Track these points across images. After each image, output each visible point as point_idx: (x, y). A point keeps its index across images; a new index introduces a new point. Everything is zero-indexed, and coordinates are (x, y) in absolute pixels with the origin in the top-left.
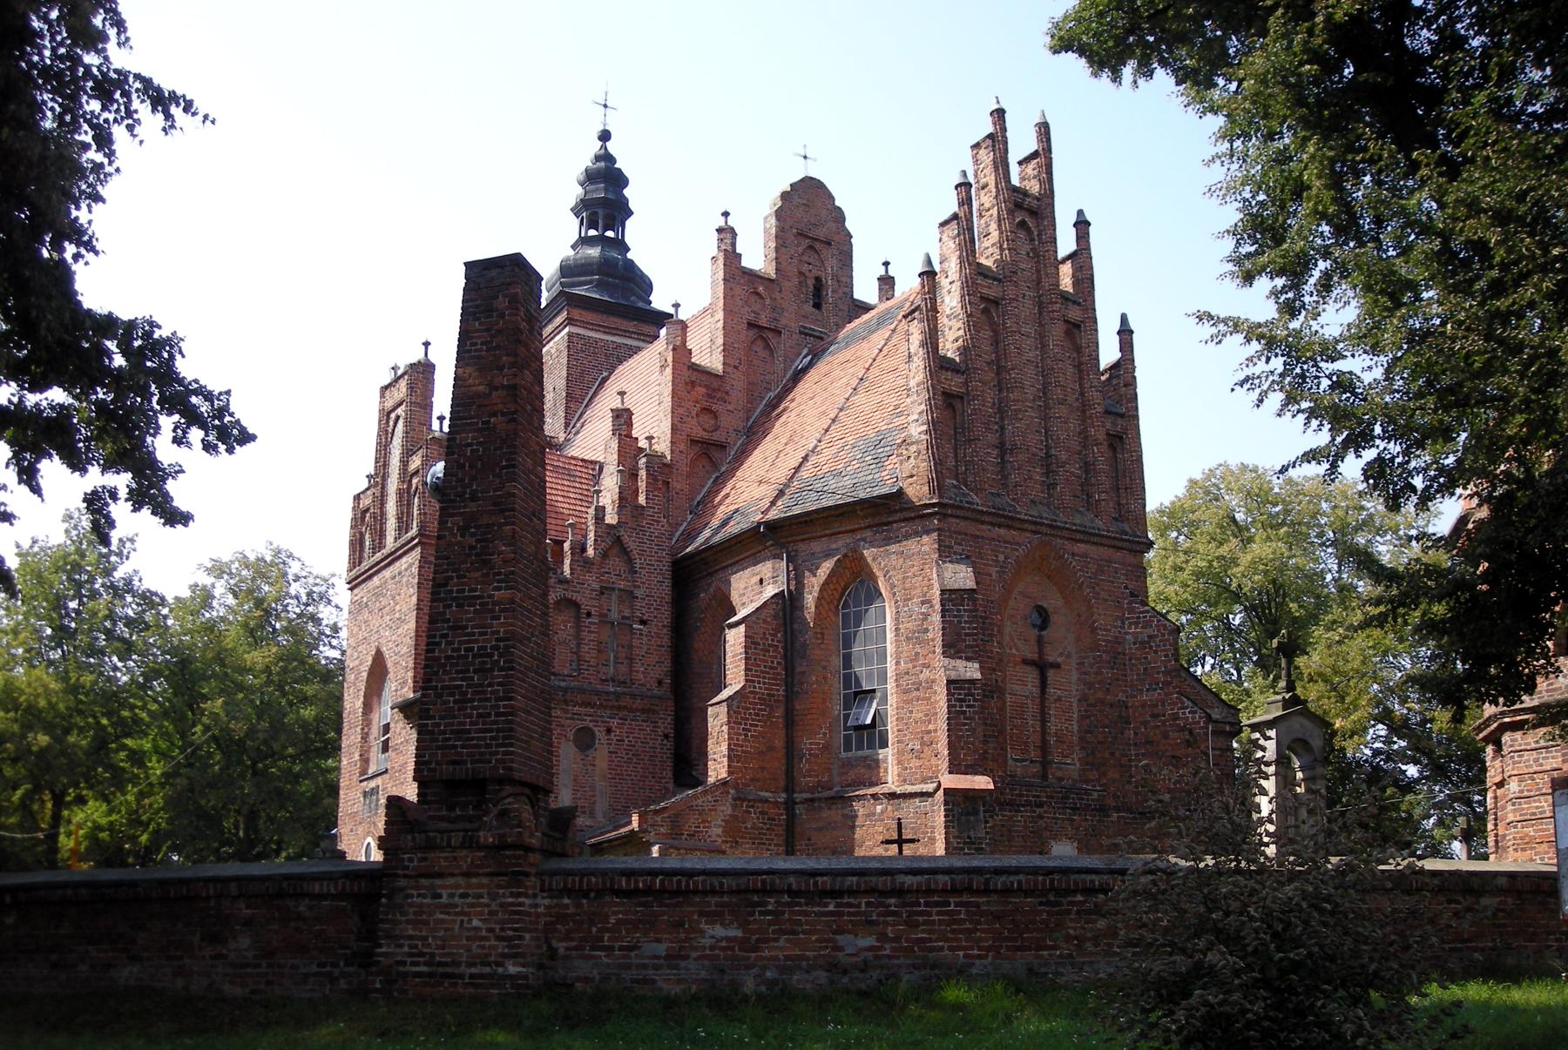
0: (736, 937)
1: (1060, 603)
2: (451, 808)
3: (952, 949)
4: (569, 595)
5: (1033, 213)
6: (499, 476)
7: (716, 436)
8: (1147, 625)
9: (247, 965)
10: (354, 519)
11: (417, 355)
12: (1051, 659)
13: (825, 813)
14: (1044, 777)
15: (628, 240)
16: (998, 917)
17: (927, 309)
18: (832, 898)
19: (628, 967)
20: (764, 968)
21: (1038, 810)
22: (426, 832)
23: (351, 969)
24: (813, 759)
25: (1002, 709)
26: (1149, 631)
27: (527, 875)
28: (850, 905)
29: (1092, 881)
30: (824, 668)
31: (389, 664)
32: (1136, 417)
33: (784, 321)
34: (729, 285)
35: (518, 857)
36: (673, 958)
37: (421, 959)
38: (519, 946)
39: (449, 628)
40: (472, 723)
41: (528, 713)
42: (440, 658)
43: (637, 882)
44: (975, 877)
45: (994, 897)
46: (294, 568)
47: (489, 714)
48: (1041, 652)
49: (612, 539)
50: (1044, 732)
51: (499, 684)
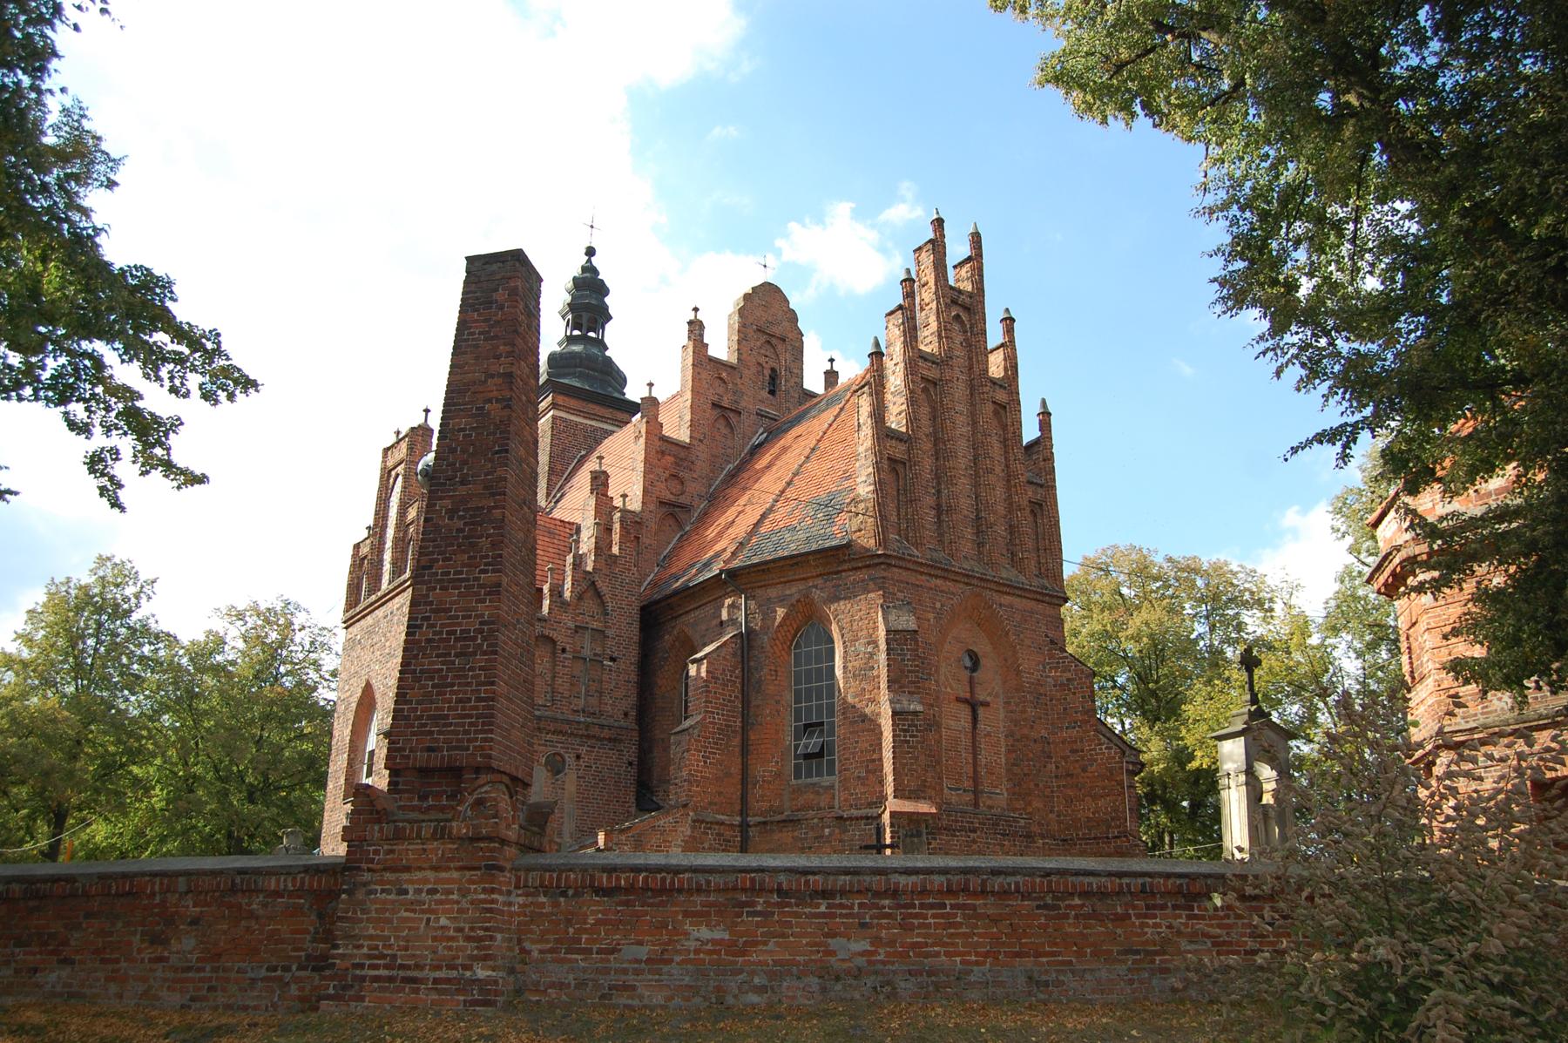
0: (723, 940)
1: (989, 648)
2: (423, 798)
3: (947, 954)
4: (546, 632)
5: (967, 309)
6: (491, 460)
7: (682, 500)
8: (1065, 670)
9: (189, 969)
10: (353, 565)
11: (418, 420)
12: (981, 698)
13: (776, 836)
14: (976, 805)
15: (606, 340)
16: (995, 921)
17: (875, 381)
18: (824, 898)
19: (606, 971)
20: (753, 973)
21: (972, 835)
22: (395, 821)
23: (303, 973)
24: (766, 785)
25: (939, 742)
26: (1068, 675)
27: (502, 869)
28: (841, 906)
29: (1090, 884)
30: (778, 702)
31: (378, 696)
32: (1054, 487)
33: (743, 404)
34: (698, 370)
35: (492, 850)
36: (656, 962)
37: (382, 962)
38: (489, 947)
39: (432, 611)
40: (449, 709)
41: (510, 700)
42: (419, 641)
43: (618, 879)
44: (971, 877)
45: (991, 900)
46: (300, 618)
47: (470, 699)
48: (972, 692)
49: (588, 585)
50: (975, 764)
51: (481, 668)
